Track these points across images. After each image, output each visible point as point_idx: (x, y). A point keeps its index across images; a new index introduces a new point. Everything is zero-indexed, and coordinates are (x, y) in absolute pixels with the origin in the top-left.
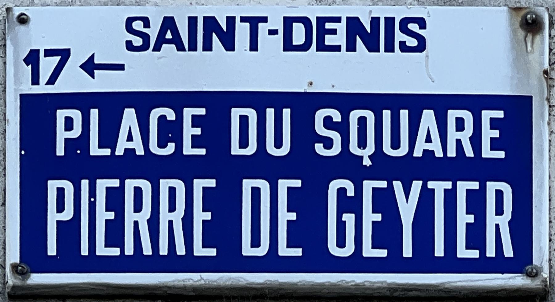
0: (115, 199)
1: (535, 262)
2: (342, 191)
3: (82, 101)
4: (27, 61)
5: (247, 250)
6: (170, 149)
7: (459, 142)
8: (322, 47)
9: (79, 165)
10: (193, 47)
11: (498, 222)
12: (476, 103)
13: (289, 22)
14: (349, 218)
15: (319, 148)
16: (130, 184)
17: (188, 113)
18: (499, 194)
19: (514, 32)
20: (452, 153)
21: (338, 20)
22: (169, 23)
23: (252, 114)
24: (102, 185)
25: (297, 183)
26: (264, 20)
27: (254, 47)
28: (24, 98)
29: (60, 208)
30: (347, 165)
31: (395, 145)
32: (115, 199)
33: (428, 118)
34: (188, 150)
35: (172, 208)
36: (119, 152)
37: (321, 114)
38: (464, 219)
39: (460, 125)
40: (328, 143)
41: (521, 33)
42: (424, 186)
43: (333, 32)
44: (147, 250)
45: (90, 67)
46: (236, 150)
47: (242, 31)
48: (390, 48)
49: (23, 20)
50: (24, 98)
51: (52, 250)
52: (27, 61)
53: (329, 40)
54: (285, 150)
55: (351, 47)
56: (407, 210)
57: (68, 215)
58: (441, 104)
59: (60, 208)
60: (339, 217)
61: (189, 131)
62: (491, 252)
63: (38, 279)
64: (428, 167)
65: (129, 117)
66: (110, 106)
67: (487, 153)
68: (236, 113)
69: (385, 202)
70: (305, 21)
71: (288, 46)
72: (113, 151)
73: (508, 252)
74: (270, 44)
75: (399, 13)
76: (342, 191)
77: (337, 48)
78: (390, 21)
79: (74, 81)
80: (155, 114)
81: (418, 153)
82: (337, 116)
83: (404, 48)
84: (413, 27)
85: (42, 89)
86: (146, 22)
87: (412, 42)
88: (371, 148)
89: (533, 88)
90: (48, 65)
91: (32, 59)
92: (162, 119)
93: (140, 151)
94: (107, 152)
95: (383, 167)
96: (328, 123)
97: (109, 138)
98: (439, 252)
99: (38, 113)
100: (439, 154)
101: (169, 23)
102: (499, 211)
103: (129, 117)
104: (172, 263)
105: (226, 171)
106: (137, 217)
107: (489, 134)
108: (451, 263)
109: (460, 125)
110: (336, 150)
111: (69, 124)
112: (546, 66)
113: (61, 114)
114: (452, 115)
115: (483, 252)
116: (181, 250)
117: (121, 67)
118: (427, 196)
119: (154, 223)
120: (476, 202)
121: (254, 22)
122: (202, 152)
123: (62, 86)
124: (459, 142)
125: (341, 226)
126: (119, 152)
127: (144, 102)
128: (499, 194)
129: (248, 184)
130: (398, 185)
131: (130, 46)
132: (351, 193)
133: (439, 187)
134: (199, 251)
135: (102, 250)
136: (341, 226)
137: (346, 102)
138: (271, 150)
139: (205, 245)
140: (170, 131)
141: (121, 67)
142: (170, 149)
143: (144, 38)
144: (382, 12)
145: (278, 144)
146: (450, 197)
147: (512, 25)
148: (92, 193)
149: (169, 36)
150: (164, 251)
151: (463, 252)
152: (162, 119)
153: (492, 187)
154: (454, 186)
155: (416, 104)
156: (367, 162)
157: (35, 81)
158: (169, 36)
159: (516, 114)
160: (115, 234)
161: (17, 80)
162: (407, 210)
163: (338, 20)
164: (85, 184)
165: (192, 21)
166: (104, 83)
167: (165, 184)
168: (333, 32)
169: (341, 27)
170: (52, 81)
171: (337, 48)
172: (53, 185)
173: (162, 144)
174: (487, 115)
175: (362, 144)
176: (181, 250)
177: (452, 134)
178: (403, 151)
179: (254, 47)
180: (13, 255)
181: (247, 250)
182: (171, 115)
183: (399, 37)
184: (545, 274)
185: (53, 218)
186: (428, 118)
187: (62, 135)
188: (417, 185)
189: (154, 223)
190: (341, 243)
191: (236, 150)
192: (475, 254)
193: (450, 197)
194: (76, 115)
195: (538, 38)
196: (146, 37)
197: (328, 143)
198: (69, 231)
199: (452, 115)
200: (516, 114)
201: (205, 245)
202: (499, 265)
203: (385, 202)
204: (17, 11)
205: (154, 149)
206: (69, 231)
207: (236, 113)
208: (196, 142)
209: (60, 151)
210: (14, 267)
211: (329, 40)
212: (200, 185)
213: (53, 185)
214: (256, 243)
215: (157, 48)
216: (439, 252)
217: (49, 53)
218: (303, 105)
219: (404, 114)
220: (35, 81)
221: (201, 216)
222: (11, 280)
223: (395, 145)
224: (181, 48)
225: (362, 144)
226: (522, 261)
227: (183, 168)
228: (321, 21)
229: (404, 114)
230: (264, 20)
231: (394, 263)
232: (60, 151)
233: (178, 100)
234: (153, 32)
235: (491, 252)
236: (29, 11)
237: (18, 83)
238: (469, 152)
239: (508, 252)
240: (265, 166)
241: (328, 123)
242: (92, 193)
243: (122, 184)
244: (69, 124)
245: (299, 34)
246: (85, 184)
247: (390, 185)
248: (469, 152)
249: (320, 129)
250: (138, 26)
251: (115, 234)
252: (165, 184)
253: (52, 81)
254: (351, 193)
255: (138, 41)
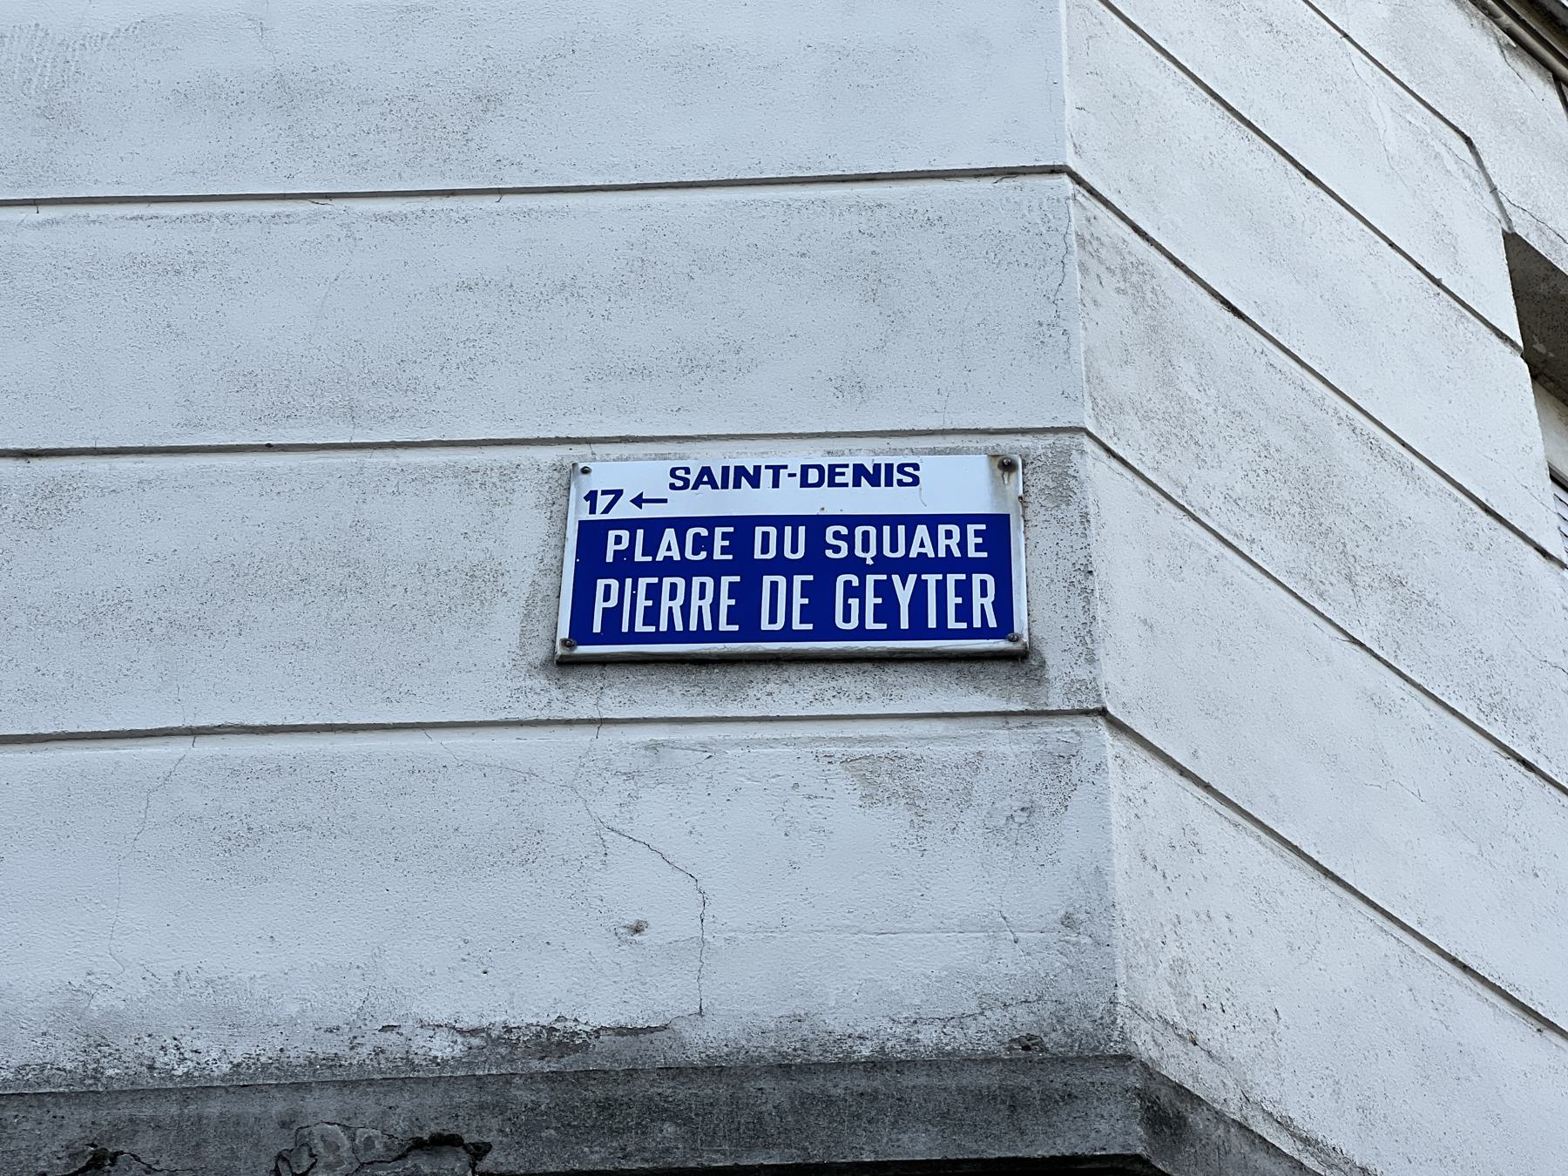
0: (654, 592)
1: (1016, 630)
2: (847, 583)
3: (631, 525)
4: (586, 498)
5: (765, 625)
6: (703, 555)
7: (948, 547)
8: (832, 484)
9: (625, 567)
10: (725, 486)
11: (983, 604)
12: (962, 520)
13: (805, 469)
14: (854, 602)
15: (829, 553)
16: (667, 581)
17: (719, 531)
18: (983, 583)
19: (993, 471)
20: (942, 553)
21: (846, 466)
22: (706, 471)
23: (773, 531)
24: (643, 582)
25: (737, 579)
26: (785, 467)
27: (776, 484)
28: (583, 525)
29: (607, 598)
30: (853, 564)
31: (894, 548)
32: (654, 592)
33: (922, 531)
34: (717, 556)
35: (702, 597)
36: (660, 558)
37: (830, 531)
38: (953, 600)
39: (949, 535)
40: (837, 549)
41: (999, 472)
42: (919, 578)
43: (843, 474)
44: (679, 627)
45: (639, 501)
46: (758, 555)
47: (766, 476)
48: (889, 483)
49: (585, 471)
50: (583, 525)
51: (597, 628)
52: (586, 498)
53: (838, 479)
54: (800, 554)
55: (857, 483)
56: (904, 595)
57: (613, 603)
58: (932, 521)
59: (607, 598)
60: (845, 601)
61: (719, 543)
62: (977, 623)
63: (583, 650)
64: (923, 564)
65: (670, 535)
66: (654, 528)
67: (972, 553)
68: (759, 530)
69: (885, 590)
70: (820, 468)
71: (804, 483)
72: (654, 557)
73: (992, 623)
74: (789, 484)
75: (896, 461)
76: (847, 583)
77: (846, 485)
78: (889, 467)
79: (624, 510)
80: (691, 533)
81: (913, 554)
82: (844, 531)
83: (901, 483)
84: (909, 470)
85: (598, 516)
86: (687, 471)
87: (909, 480)
88: (873, 551)
89: (1010, 508)
90: (602, 502)
91: (592, 497)
92: (697, 536)
93: (677, 557)
94: (649, 559)
95: (881, 564)
96: (837, 535)
97: (651, 547)
98: (932, 623)
99: (591, 535)
100: (931, 555)
101: (706, 471)
102: (984, 594)
103: (670, 535)
104: (700, 636)
105: (748, 572)
106: (983, 600)
107: (972, 541)
108: (942, 632)
109: (949, 535)
110: (844, 553)
111: (618, 540)
112: (1021, 493)
113: (612, 534)
114: (942, 529)
115: (970, 623)
116: (708, 626)
117: (665, 501)
118: (921, 587)
119: (686, 609)
120: (964, 589)
121: (776, 470)
122: (985, 555)
123: (614, 515)
124: (948, 547)
125: (847, 608)
126: (660, 558)
127: (681, 525)
128: (983, 583)
129: (767, 580)
130: (896, 578)
131: (672, 486)
132: (856, 583)
133: (932, 579)
134: (723, 626)
135: (640, 627)
136: (847, 608)
137: (852, 521)
138: (788, 554)
139: (957, 620)
140: (703, 544)
141: (665, 501)
142: (703, 555)
143: (681, 480)
144: (883, 460)
145: (794, 550)
146: (941, 587)
147: (991, 466)
148: (635, 587)
149: (705, 479)
150: (693, 627)
151: (952, 624)
152: (697, 536)
153: (977, 578)
154: (945, 578)
155: (911, 522)
156: (869, 562)
157: (593, 510)
158: (705, 479)
159: (996, 530)
160: (652, 616)
161: (577, 511)
162: (904, 595)
163: (846, 466)
164: (629, 582)
165: (725, 470)
166: (649, 512)
167: (696, 581)
168: (843, 474)
169: (849, 472)
170: (606, 511)
171: (846, 485)
172: (601, 583)
173: (695, 552)
174: (971, 528)
175: (866, 548)
176: (708, 626)
177: (942, 542)
178: (901, 553)
179: (776, 484)
180: (564, 632)
181: (765, 625)
182: (704, 532)
183: (897, 476)
184: (1026, 639)
185: (600, 605)
186: (922, 531)
187: (611, 548)
188: (912, 578)
189: (686, 609)
190: (847, 619)
191: (758, 555)
192: (964, 626)
193: (941, 587)
194: (625, 534)
195: (1013, 476)
196: (686, 482)
197: (837, 549)
198: (612, 616)
199: (942, 529)
200: (996, 530)
201: (957, 620)
202: (985, 632)
203: (885, 590)
204: (581, 466)
205: (689, 555)
206: (612, 616)
207: (759, 530)
208: (724, 550)
209: (610, 558)
210: (564, 642)
211: (838, 479)
212: (725, 581)
213: (601, 583)
214: (773, 620)
215: (695, 487)
216: (932, 623)
217: (604, 493)
218: (817, 524)
219: (901, 529)
220: (593, 510)
221: (726, 602)
222: (560, 651)
223: (894, 548)
224: (715, 486)
225: (866, 548)
226: (1005, 626)
227: (714, 569)
228: (832, 467)
229: (901, 529)
230: (785, 467)
231: (894, 633)
232: (610, 558)
233: (711, 522)
234: (693, 478)
235: (977, 623)
236: (590, 465)
237: (579, 512)
238: (957, 553)
239: (992, 623)
240: (781, 566)
241: (837, 535)
242: (635, 587)
243: (661, 582)
244: (618, 540)
245: (813, 476)
246: (629, 582)
247: (890, 580)
248: (957, 553)
249: (830, 539)
250: (680, 473)
251: (652, 616)
252: (696, 581)
253: (606, 511)
254: (856, 583)
255: (679, 483)
